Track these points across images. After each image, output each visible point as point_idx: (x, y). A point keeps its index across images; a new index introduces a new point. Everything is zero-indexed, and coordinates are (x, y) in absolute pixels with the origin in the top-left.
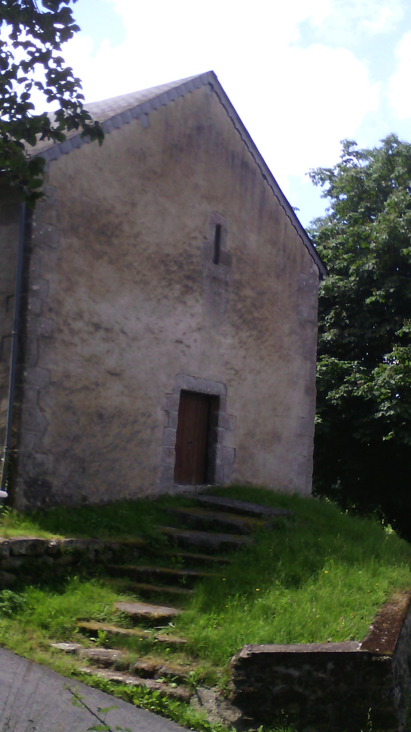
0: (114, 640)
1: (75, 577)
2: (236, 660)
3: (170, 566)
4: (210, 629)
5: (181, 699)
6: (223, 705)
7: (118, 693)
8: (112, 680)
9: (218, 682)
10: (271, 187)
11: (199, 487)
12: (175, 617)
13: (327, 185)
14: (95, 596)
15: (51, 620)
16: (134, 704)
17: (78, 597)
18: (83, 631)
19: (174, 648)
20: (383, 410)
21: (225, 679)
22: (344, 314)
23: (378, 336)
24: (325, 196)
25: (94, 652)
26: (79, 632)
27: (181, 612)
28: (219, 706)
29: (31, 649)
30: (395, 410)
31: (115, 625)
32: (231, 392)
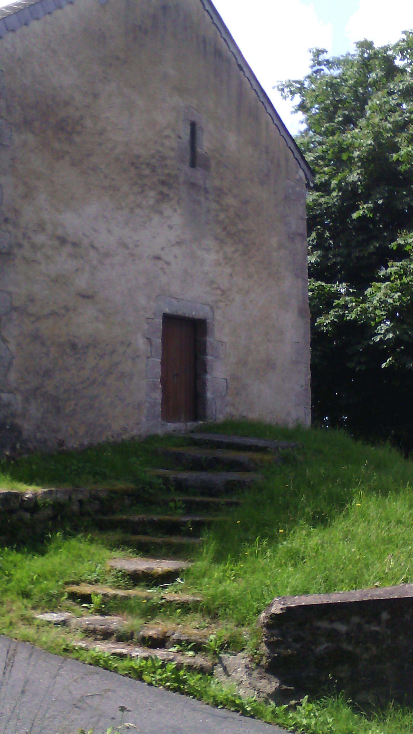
0: (112, 604)
1: (58, 534)
2: (266, 618)
3: (169, 513)
4: (228, 581)
5: (202, 670)
6: (255, 673)
7: (123, 670)
8: (114, 654)
9: (246, 645)
10: (249, 80)
11: (189, 424)
12: (183, 571)
13: (298, 99)
14: (83, 553)
15: (32, 586)
16: (144, 682)
17: (64, 557)
18: (73, 596)
19: (186, 608)
20: (380, 334)
21: (254, 641)
22: (327, 234)
23: (366, 255)
24: (296, 111)
25: (88, 621)
26: (68, 598)
27: (190, 565)
28: (250, 674)
29: (11, 623)
30: (394, 333)
31: (111, 587)
32: (218, 315)
